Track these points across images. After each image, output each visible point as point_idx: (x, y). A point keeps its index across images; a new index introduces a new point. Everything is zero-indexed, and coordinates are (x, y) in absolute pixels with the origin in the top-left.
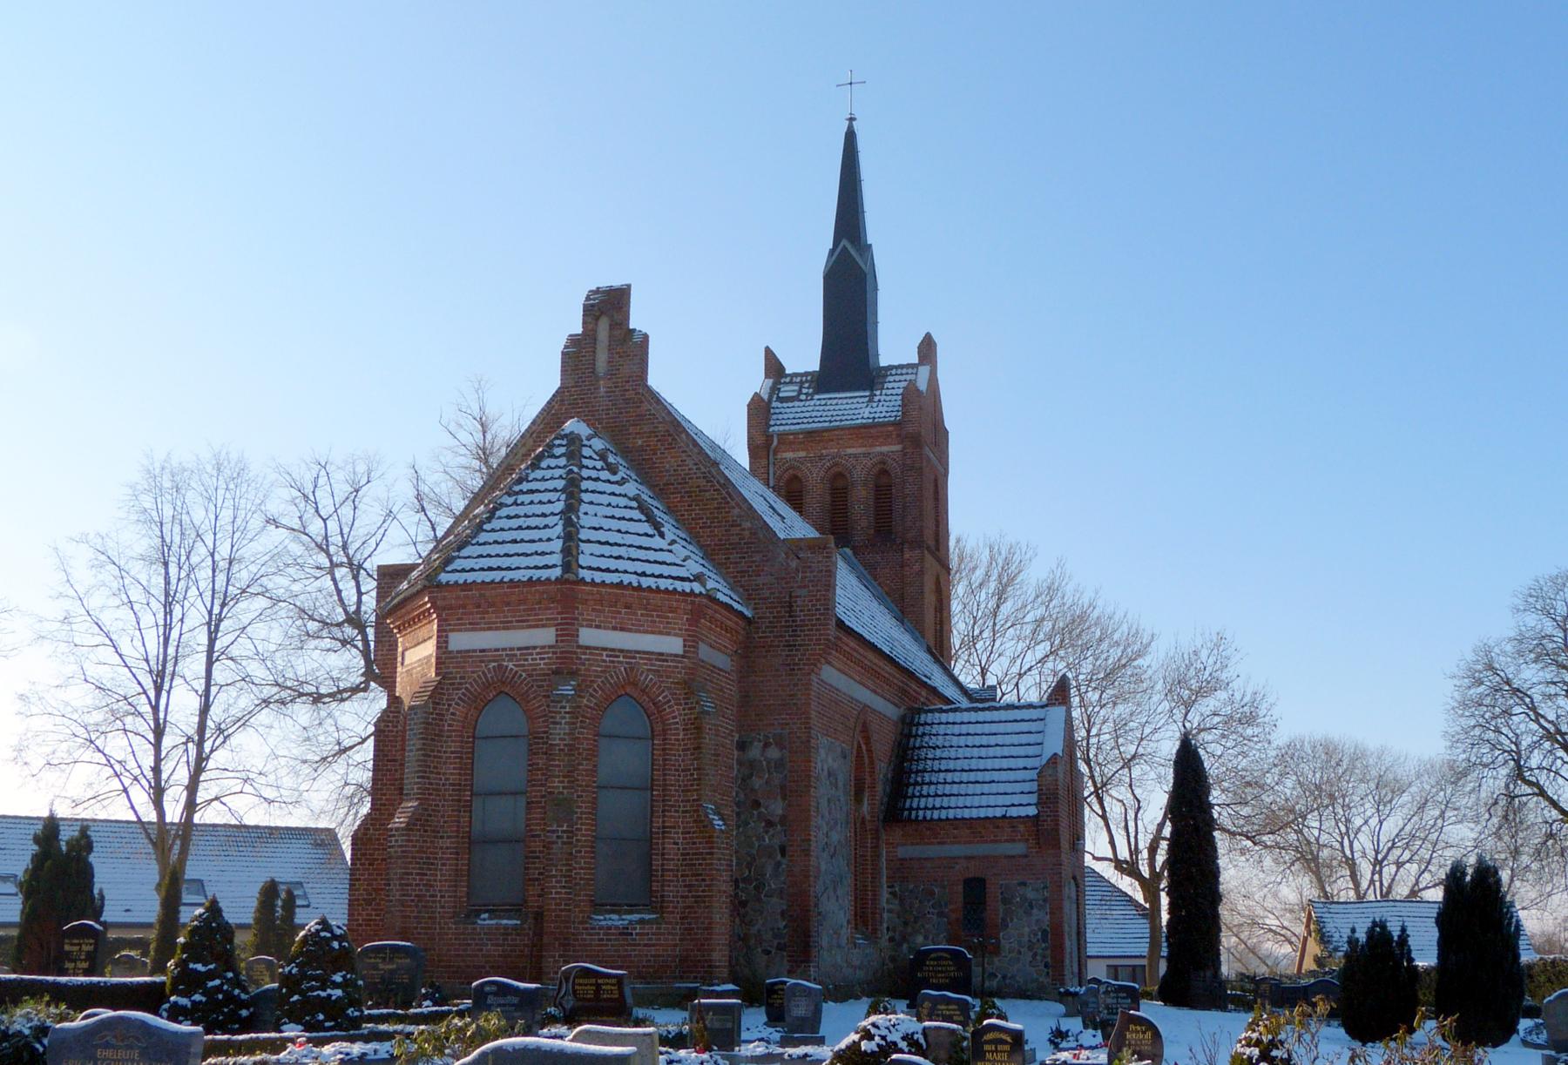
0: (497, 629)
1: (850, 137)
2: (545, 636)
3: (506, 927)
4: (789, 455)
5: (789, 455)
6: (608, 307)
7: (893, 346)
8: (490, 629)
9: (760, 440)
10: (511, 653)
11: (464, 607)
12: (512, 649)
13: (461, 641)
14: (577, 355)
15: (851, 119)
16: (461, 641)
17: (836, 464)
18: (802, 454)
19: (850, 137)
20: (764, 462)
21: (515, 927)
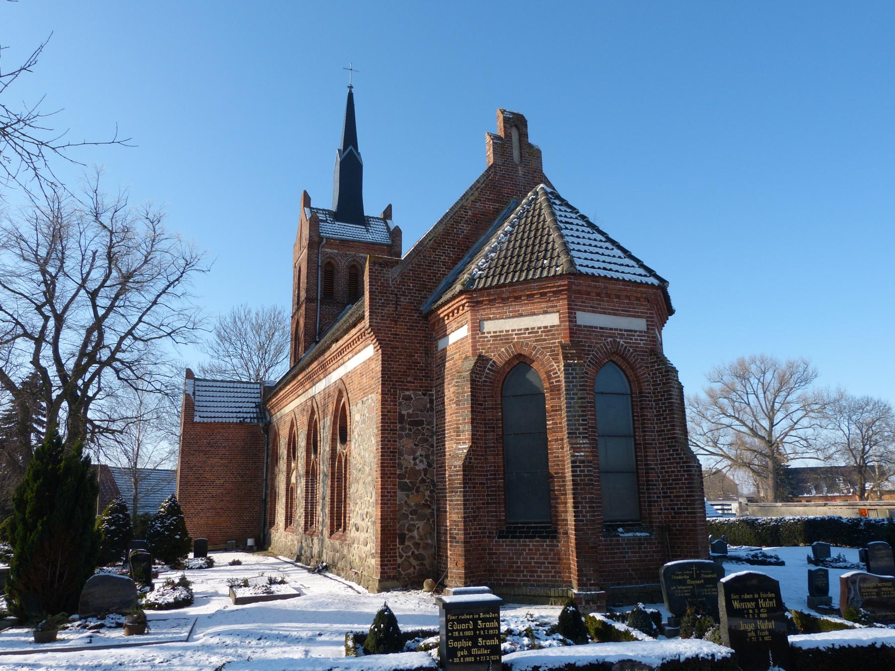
0: (609, 314)
1: (350, 97)
2: (640, 324)
3: (640, 538)
4: (328, 250)
5: (328, 250)
6: (516, 123)
7: (372, 207)
8: (605, 313)
9: (316, 239)
10: (520, 332)
11: (588, 293)
12: (621, 330)
13: (585, 318)
14: (501, 145)
15: (351, 87)
16: (585, 318)
17: (354, 260)
18: (336, 251)
19: (350, 97)
20: (316, 251)
21: (646, 538)
